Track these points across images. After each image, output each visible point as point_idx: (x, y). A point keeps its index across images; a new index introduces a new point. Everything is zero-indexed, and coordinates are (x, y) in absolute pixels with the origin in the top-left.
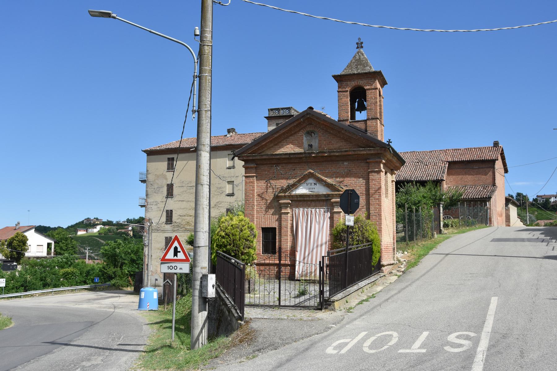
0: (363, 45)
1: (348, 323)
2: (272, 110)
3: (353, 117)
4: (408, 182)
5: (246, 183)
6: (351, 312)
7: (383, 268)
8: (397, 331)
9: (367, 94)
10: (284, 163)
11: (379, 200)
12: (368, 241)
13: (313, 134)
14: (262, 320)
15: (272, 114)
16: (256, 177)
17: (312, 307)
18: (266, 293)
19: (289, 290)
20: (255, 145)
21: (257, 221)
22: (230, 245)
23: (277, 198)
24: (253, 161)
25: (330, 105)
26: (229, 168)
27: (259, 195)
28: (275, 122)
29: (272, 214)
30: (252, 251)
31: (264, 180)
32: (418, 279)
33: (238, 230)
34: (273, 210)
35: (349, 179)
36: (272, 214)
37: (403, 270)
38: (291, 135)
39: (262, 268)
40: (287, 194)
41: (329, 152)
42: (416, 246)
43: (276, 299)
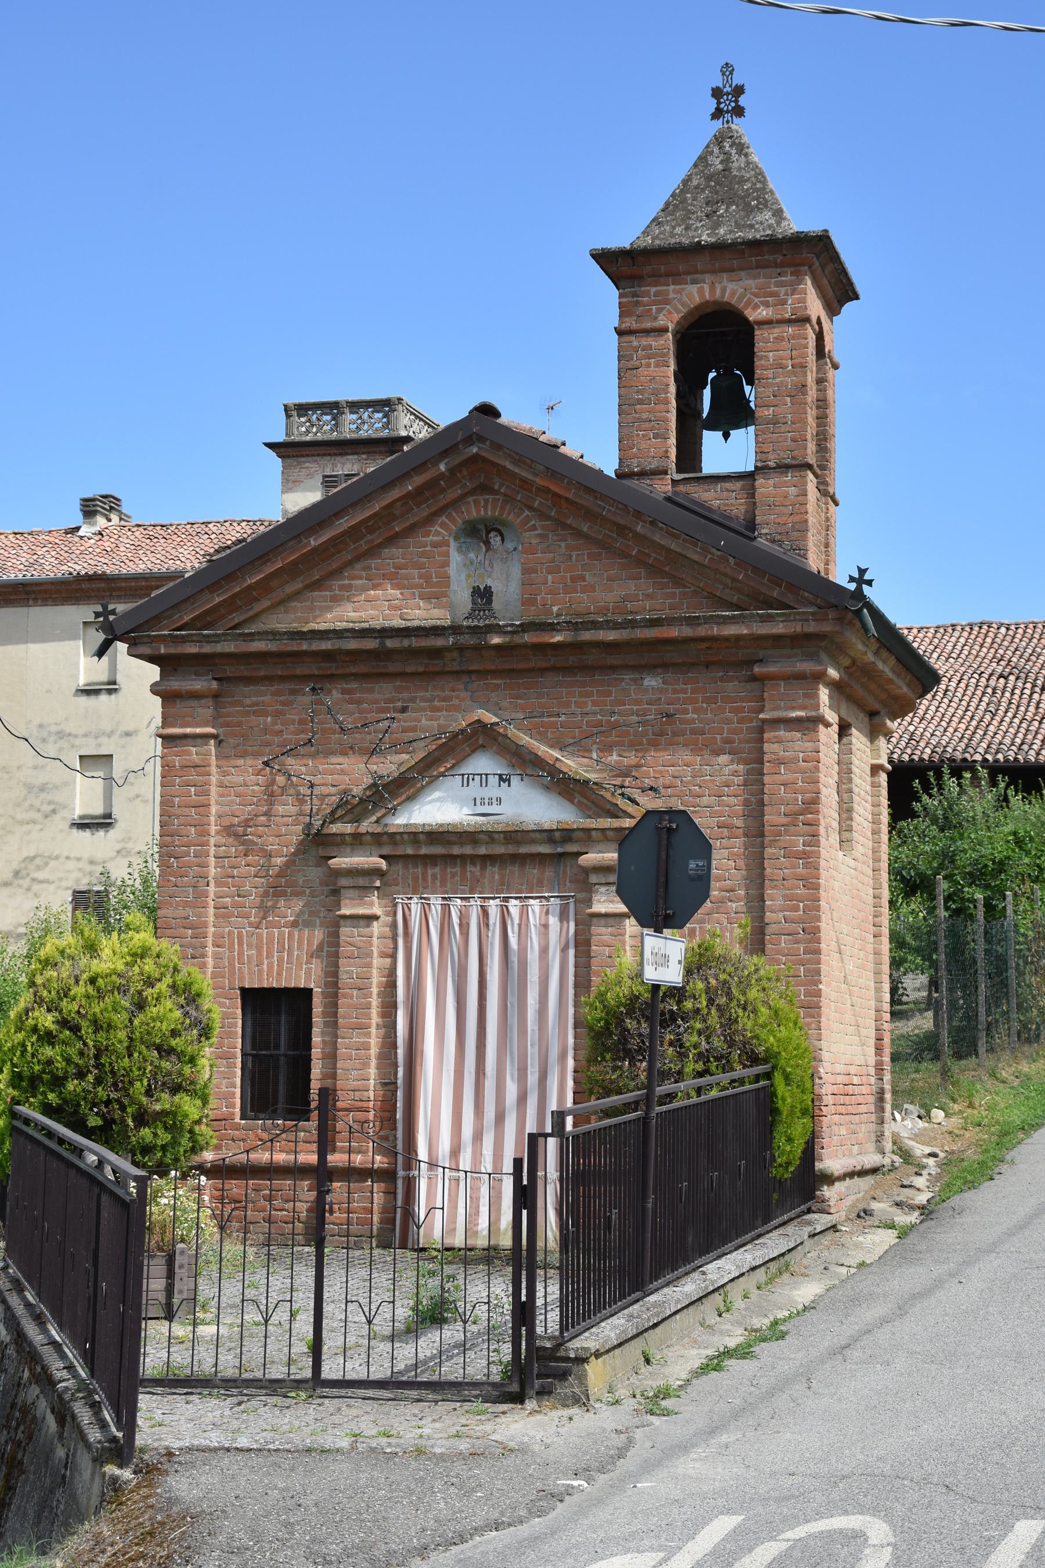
0: (743, 101)
1: (648, 1467)
2: (303, 409)
3: (689, 455)
4: (958, 768)
5: (168, 772)
6: (666, 1413)
7: (827, 1192)
8: (888, 1517)
9: (759, 345)
10: (356, 676)
11: (810, 858)
12: (754, 1059)
13: (495, 540)
14: (226, 1460)
15: (303, 431)
16: (220, 743)
17: (475, 1385)
18: (252, 1316)
19: (365, 1304)
20: (214, 587)
21: (217, 957)
22: (81, 1075)
23: (318, 843)
24: (202, 662)
25: (580, 405)
26: (89, 692)
27: (228, 830)
28: (317, 469)
29: (294, 924)
30: (189, 1106)
31: (256, 755)
32: (992, 1248)
33: (126, 1004)
34: (298, 905)
35: (665, 756)
36: (294, 924)
37: (922, 1198)
38: (392, 540)
39: (235, 1187)
40: (367, 826)
41: (575, 627)
42: (989, 1083)
43: (301, 1348)
